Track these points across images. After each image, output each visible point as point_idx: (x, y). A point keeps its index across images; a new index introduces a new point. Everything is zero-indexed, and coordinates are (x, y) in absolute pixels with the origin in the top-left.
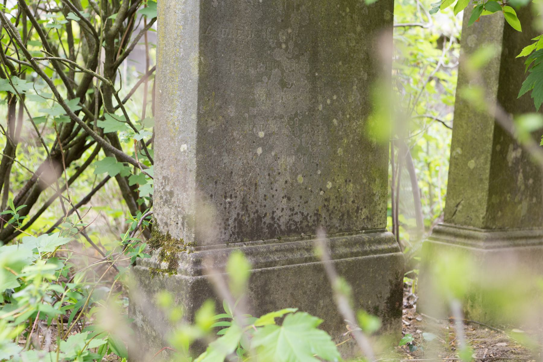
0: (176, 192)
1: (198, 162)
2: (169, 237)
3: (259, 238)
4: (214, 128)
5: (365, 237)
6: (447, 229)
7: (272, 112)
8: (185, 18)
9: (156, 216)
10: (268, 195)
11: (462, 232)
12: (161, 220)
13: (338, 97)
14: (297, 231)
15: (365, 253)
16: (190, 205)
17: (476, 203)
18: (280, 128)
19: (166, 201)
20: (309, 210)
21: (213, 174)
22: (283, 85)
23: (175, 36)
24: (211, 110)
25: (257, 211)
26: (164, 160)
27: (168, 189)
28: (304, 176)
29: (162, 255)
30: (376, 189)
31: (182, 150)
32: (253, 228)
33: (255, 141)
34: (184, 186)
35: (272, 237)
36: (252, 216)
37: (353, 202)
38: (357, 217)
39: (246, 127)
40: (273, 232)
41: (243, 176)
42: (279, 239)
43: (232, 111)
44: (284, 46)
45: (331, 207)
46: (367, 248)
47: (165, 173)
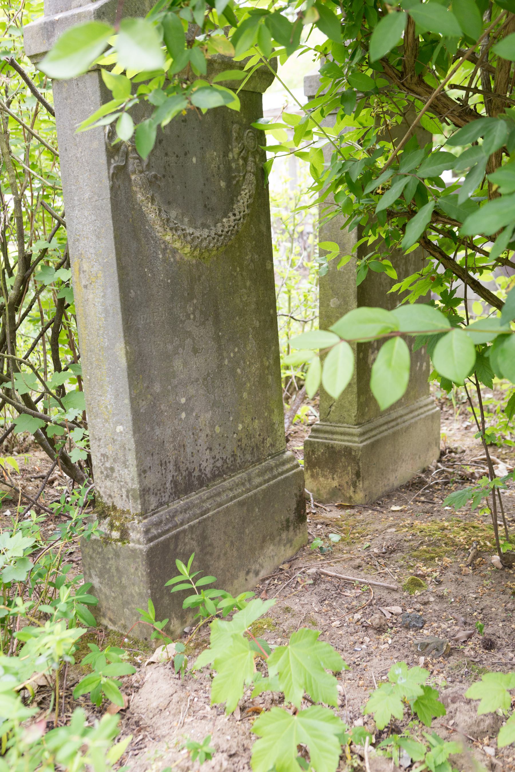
0: (116, 468)
1: (136, 442)
2: (114, 508)
3: (192, 490)
4: (145, 407)
5: (272, 462)
6: (324, 428)
7: (190, 378)
8: (106, 311)
9: (98, 489)
10: (194, 451)
11: (337, 429)
12: (105, 492)
13: (239, 348)
14: (220, 475)
15: (275, 477)
16: (133, 480)
17: (347, 404)
18: (197, 390)
19: (107, 476)
20: (226, 455)
21: (149, 448)
22: (195, 351)
23: (97, 327)
24: (141, 391)
25: (187, 469)
26: (100, 440)
27: (108, 465)
28: (220, 426)
29: (112, 526)
30: (275, 419)
31: (118, 431)
32: (186, 484)
33: (179, 408)
34: (124, 463)
35: (201, 486)
36: (184, 474)
37: (260, 435)
38: (263, 447)
39: (171, 398)
40: (203, 482)
41: (173, 442)
42: (207, 486)
43: (157, 388)
44: (192, 317)
45: (243, 445)
46: (275, 472)
47: (102, 451)
